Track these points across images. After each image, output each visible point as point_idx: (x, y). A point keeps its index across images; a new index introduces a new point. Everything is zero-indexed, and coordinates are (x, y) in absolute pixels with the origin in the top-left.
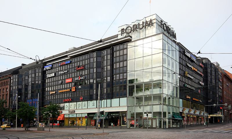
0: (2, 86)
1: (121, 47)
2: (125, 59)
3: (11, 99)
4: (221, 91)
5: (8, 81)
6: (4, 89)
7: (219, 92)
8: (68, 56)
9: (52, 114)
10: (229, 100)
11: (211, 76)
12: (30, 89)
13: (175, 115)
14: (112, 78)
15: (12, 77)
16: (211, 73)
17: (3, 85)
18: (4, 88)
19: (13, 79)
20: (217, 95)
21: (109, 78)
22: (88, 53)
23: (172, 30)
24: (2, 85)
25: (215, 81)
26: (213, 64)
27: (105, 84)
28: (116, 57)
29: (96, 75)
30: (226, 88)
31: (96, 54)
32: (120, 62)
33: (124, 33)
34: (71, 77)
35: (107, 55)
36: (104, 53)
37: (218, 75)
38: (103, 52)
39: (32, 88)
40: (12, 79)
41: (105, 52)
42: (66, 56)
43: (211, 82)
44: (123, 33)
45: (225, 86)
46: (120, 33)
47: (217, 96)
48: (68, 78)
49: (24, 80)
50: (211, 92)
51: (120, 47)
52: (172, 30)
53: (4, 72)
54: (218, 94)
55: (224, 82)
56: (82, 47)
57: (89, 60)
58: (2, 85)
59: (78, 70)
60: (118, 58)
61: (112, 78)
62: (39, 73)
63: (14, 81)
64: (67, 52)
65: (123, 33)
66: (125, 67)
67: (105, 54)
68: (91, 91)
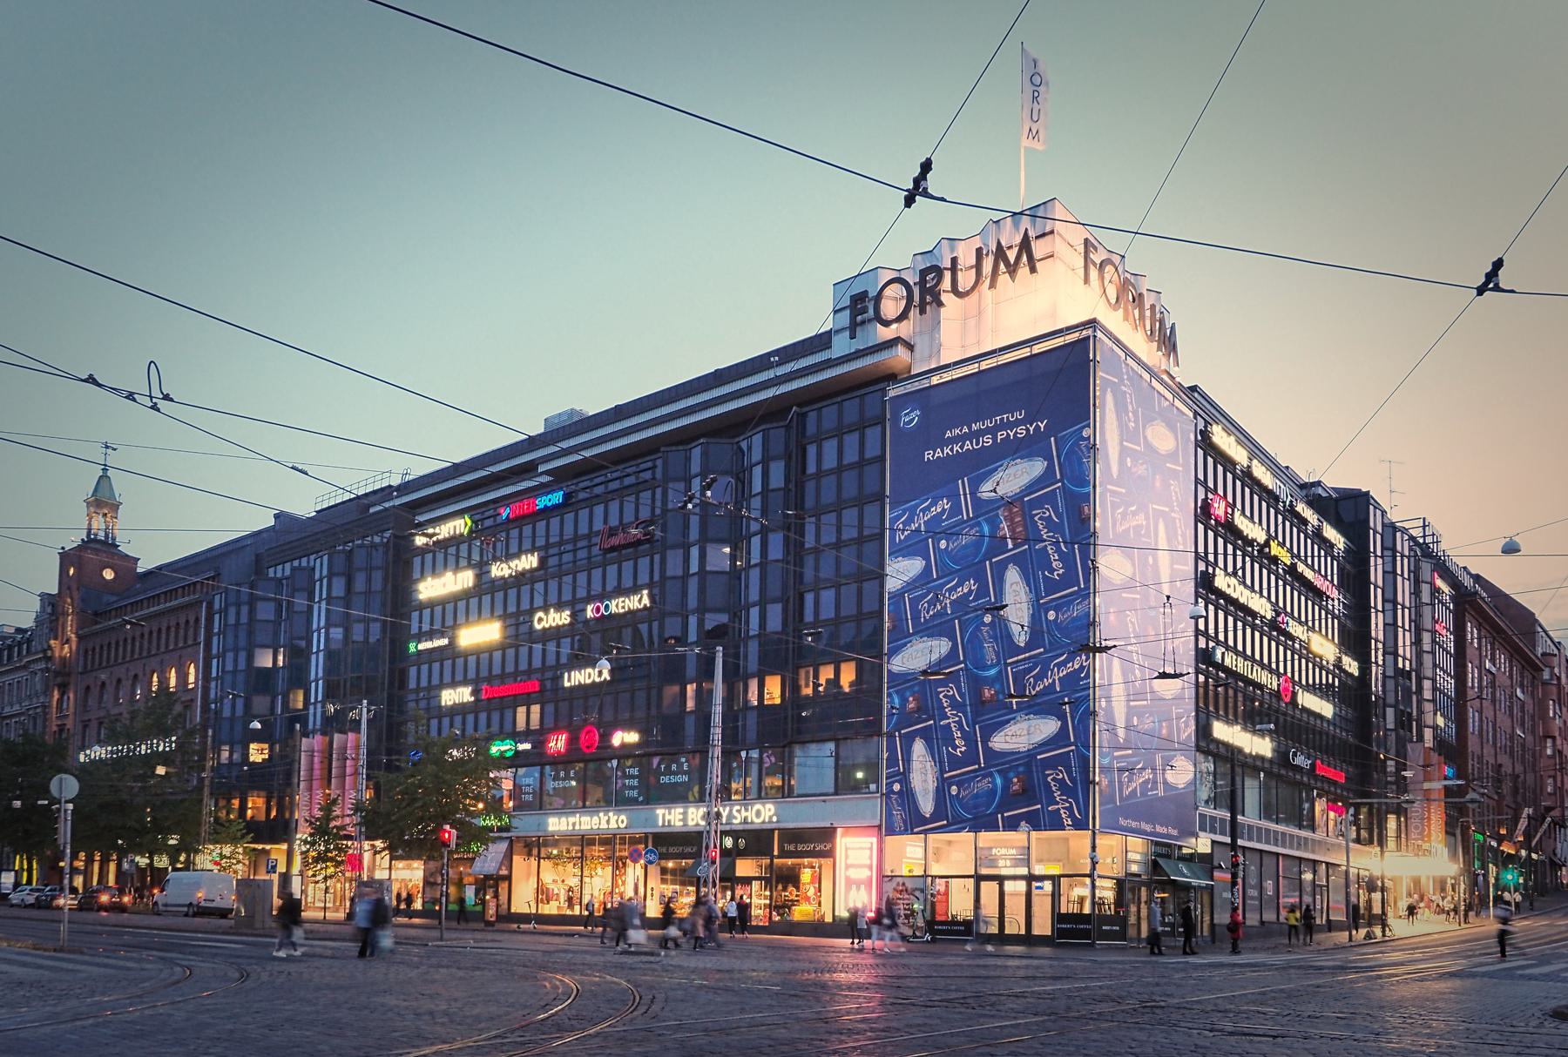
0: (163, 649)
1: (851, 410)
2: (870, 487)
3: (214, 733)
4: (1449, 664)
5: (197, 620)
6: (119, 681)
7: (1435, 666)
8: (541, 469)
9: (457, 829)
10: (1500, 765)
11: (1389, 606)
12: (320, 674)
13: (1168, 856)
14: (794, 613)
15: (217, 598)
16: (1390, 643)
17: (100, 664)
18: (108, 682)
19: (224, 612)
20: (1427, 684)
21: (775, 613)
22: (657, 451)
23: (1153, 307)
24: (129, 654)
25: (1417, 642)
26: (1404, 531)
27: (753, 648)
28: (820, 474)
29: (702, 590)
30: (1480, 687)
31: (705, 454)
32: (838, 507)
33: (870, 320)
34: (567, 596)
35: (765, 462)
36: (750, 448)
37: (1433, 653)
38: (744, 445)
39: (328, 671)
40: (217, 606)
41: (757, 440)
42: (529, 469)
43: (1392, 651)
44: (863, 322)
45: (1472, 674)
46: (845, 318)
47: (1427, 695)
48: (609, 588)
49: (288, 618)
50: (1390, 712)
51: (862, 405)
52: (1153, 307)
53: (185, 559)
54: (1434, 680)
55: (1471, 653)
56: (620, 412)
57: (659, 491)
58: (129, 654)
59: (613, 549)
60: (829, 483)
61: (794, 613)
62: (369, 569)
63: (232, 620)
64: (532, 443)
65: (863, 322)
66: (871, 538)
67: (757, 455)
68: (672, 690)
